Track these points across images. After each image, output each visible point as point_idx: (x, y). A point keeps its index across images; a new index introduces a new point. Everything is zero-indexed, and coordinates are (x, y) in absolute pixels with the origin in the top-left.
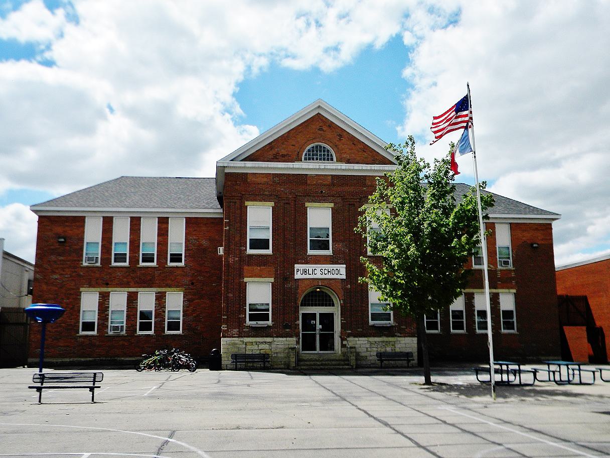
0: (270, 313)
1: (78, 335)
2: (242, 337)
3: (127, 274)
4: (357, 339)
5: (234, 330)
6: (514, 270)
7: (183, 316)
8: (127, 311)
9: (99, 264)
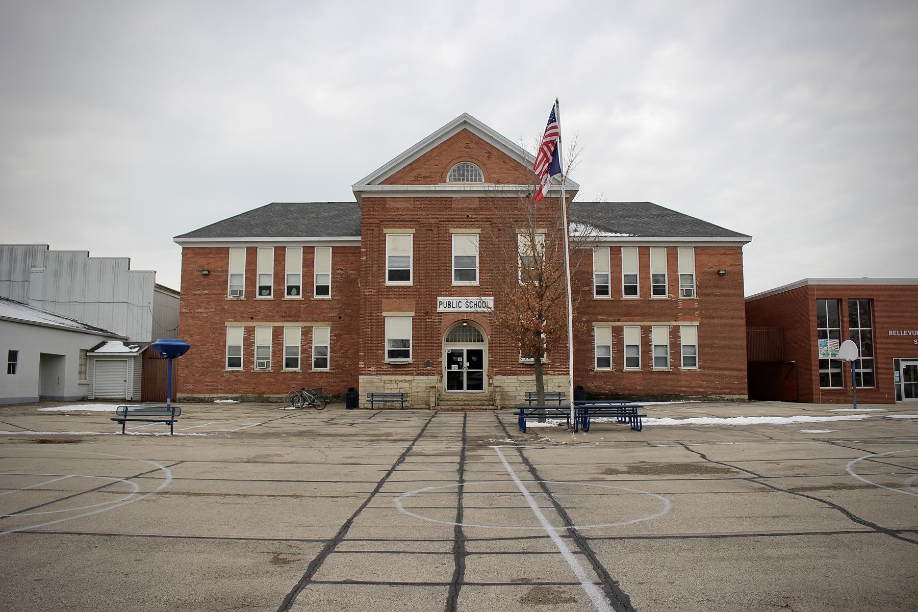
0: (411, 349)
1: (224, 370)
3: (272, 307)
4: (505, 377)
5: (372, 368)
9: (243, 298)
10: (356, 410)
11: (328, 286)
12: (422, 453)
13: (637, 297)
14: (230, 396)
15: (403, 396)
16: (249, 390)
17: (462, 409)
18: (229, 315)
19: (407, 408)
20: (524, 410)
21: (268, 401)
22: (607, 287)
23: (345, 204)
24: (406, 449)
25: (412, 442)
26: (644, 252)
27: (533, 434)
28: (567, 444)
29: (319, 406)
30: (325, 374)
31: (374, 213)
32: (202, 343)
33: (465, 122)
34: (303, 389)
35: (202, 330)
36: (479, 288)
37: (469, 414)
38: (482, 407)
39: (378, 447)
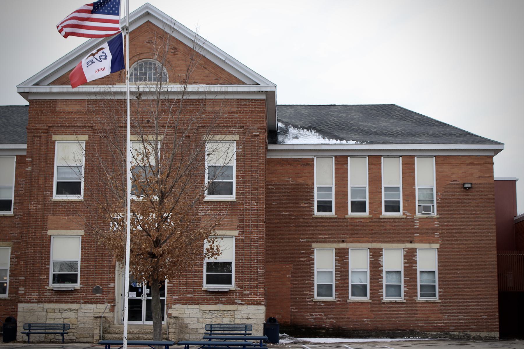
0: (233, 274)
2: (42, 302)
4: (185, 307)
5: (33, 294)
6: (438, 218)
7: (10, 277)
11: (365, 201)
13: (366, 214)
15: (65, 328)
31: (43, 118)
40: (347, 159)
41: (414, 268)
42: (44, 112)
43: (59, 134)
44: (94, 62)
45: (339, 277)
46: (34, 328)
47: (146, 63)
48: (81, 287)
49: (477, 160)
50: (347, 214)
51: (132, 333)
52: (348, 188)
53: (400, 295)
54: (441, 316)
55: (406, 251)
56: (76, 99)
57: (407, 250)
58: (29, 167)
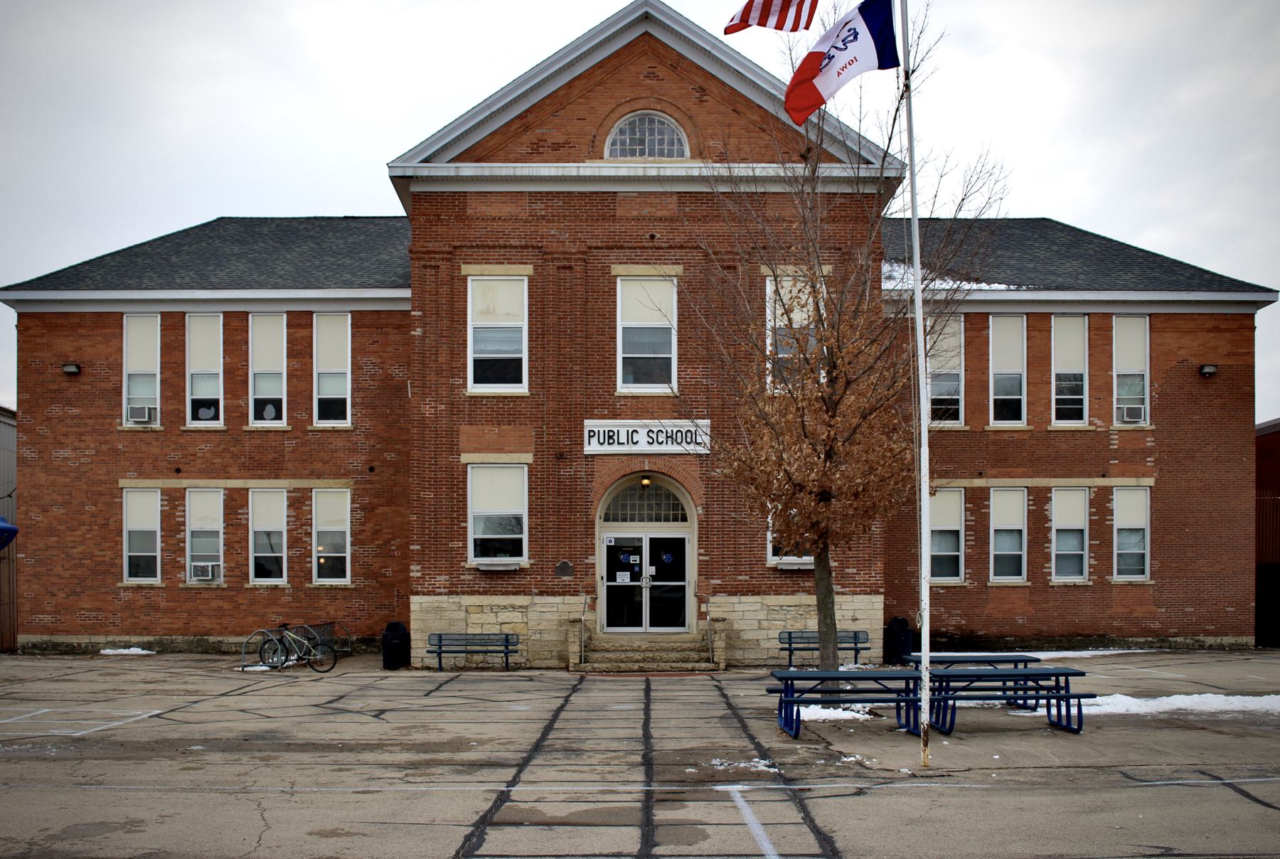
0: (525, 537)
1: (119, 585)
2: (457, 593)
3: (222, 447)
4: (734, 599)
5: (439, 578)
6: (1152, 431)
8: (224, 533)
9: (157, 425)
10: (403, 673)
11: (1019, 401)
12: (533, 811)
14: (135, 639)
15: (508, 641)
16: (175, 626)
17: (641, 670)
18: (128, 463)
19: (518, 667)
20: (795, 682)
21: (219, 650)
22: (957, 402)
23: (382, 221)
24: (494, 796)
25: (513, 771)
26: (1039, 325)
27: (817, 742)
28: (914, 776)
29: (321, 663)
30: (341, 592)
32: (69, 525)
33: (647, 18)
34: (285, 626)
35: (67, 497)
36: (677, 401)
37: (657, 683)
38: (684, 665)
39: (423, 788)
40: (988, 319)
41: (1107, 523)
42: (442, 217)
43: (474, 263)
44: (833, 57)
45: (973, 540)
46: (447, 642)
47: (642, 120)
48: (531, 564)
49: (1225, 322)
50: (988, 424)
51: (637, 651)
52: (989, 374)
53: (1081, 573)
54: (1154, 608)
55: (1094, 492)
56: (506, 192)
57: (1096, 489)
58: (418, 330)
